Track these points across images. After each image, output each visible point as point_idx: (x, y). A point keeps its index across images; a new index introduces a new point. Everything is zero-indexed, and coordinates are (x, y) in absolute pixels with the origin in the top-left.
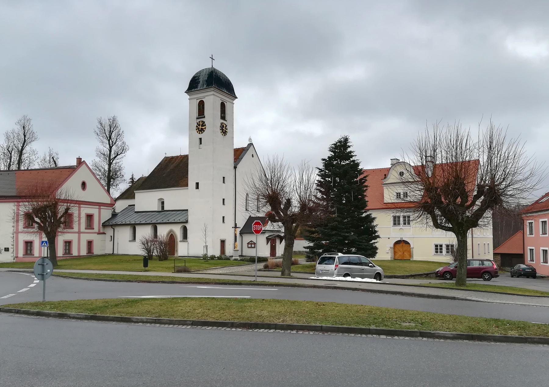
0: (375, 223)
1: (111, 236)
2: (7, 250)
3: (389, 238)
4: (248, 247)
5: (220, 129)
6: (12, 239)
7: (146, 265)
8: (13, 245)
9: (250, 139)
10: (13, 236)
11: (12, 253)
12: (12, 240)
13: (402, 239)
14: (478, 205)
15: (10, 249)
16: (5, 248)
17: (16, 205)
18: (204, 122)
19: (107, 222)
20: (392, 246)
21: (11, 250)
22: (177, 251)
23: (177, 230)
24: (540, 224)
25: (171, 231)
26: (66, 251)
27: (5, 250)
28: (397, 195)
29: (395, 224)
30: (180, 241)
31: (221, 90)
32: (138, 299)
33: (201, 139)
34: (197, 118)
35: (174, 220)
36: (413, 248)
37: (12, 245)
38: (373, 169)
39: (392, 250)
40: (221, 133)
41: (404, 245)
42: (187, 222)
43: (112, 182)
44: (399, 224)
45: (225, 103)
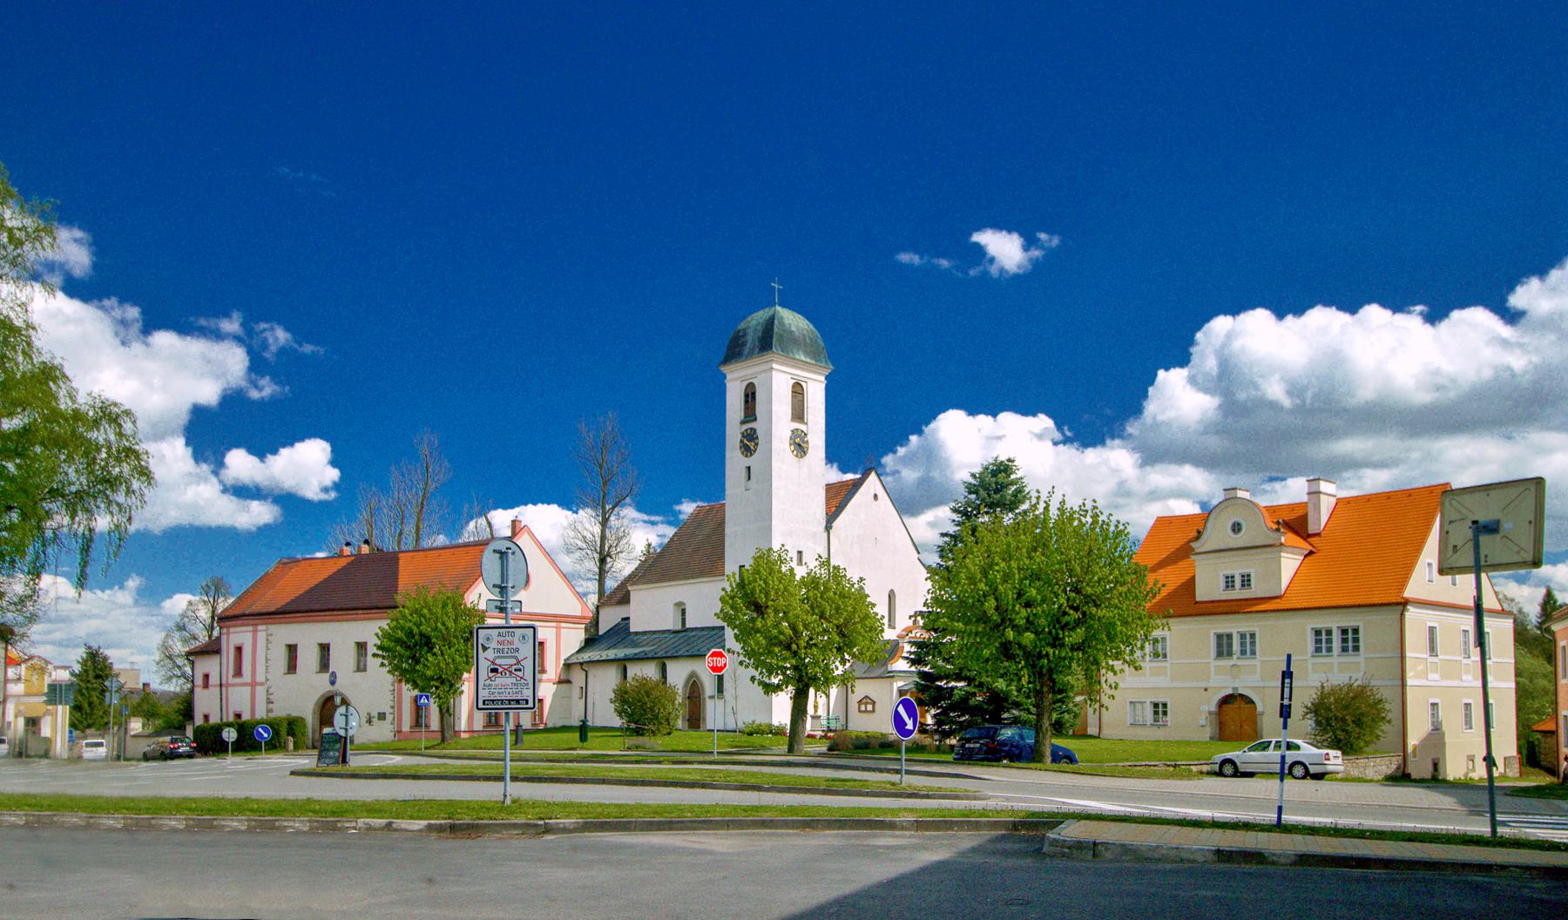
1: (582, 688)
2: (382, 716)
3: (1206, 690)
4: (860, 711)
5: (791, 445)
7: (583, 738)
8: (393, 707)
10: (392, 688)
13: (1235, 692)
16: (379, 713)
18: (755, 430)
19: (573, 658)
20: (1213, 707)
21: (389, 718)
22: (704, 719)
25: (693, 675)
26: (490, 720)
27: (379, 719)
28: (1227, 582)
29: (1220, 654)
30: (712, 697)
31: (792, 356)
34: (743, 423)
35: (698, 650)
36: (1262, 713)
39: (1214, 717)
40: (793, 452)
41: (1243, 705)
43: (609, 565)
44: (1230, 654)
45: (803, 384)
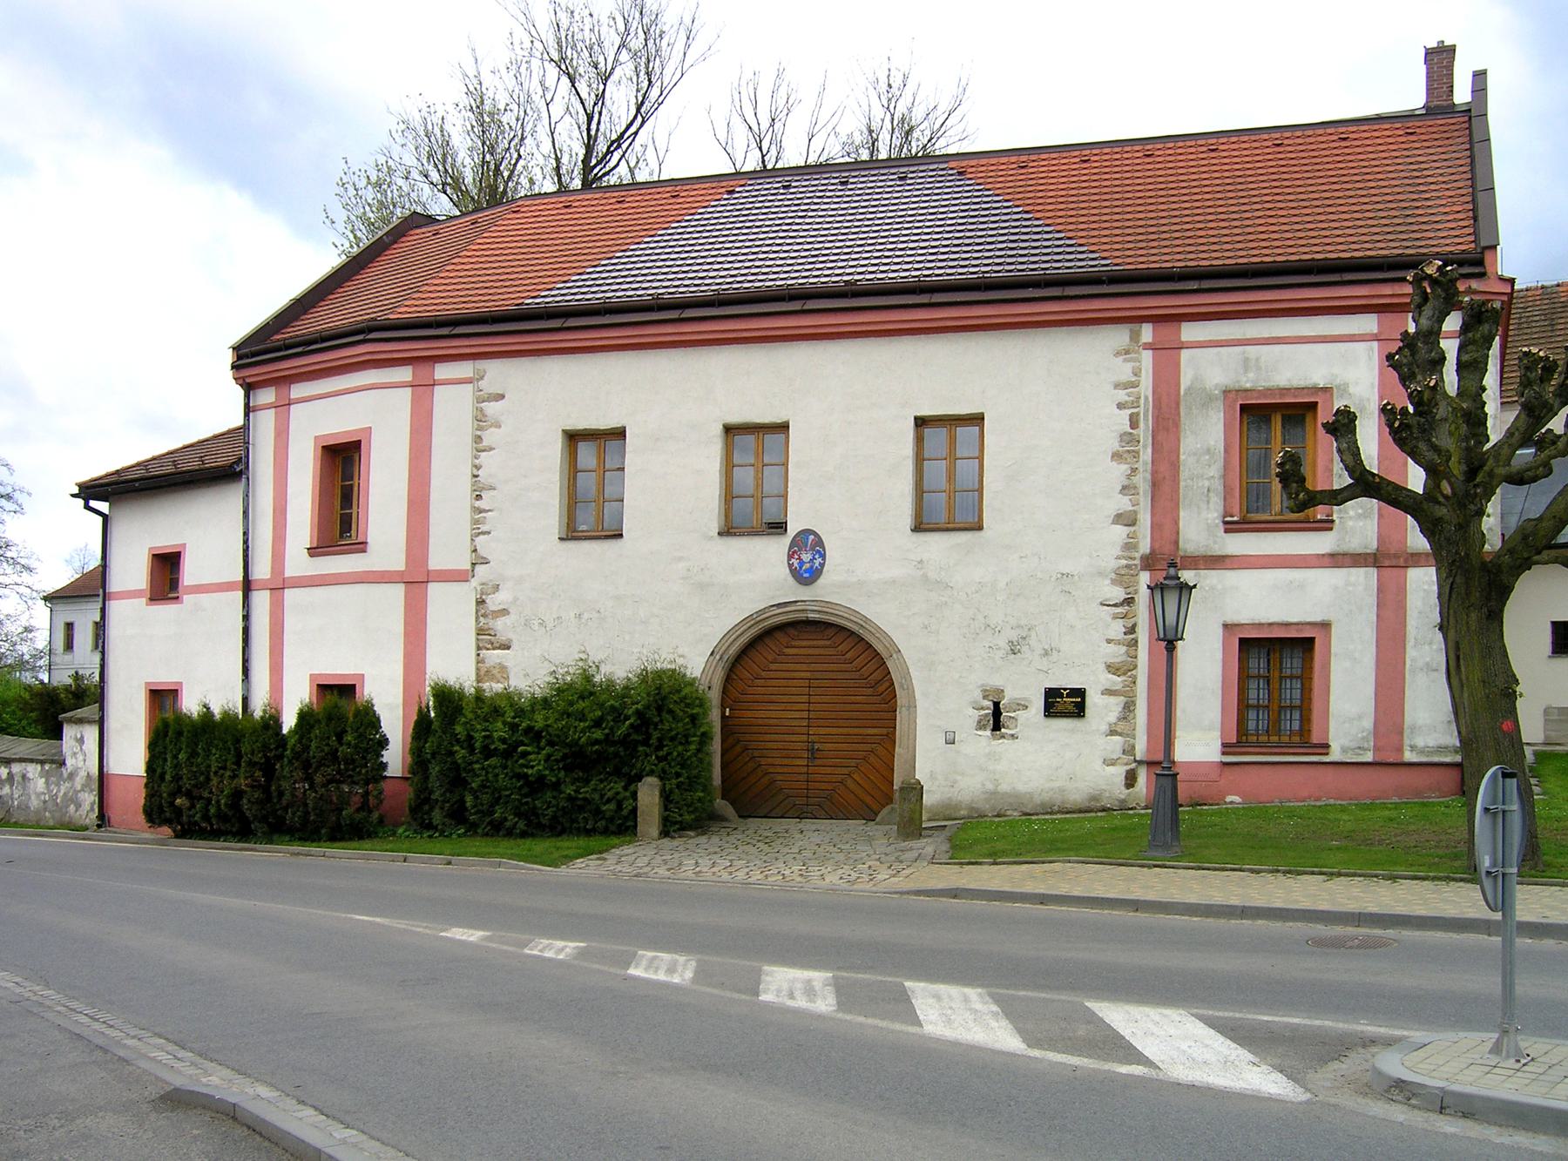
0: (217, 711)
6: (1115, 617)
11: (1112, 733)
12: (1117, 629)
15: (1093, 700)
17: (1147, 347)
21: (1102, 709)
32: (542, 836)
37: (1112, 669)
38: (180, 445)
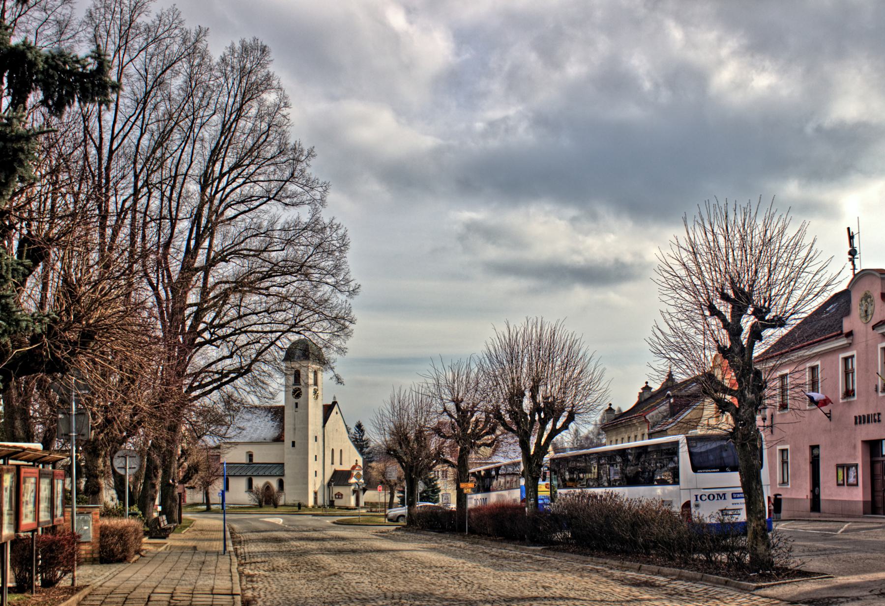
7: (299, 508)
9: (334, 398)
14: (274, 312)
23: (274, 483)
24: (778, 454)
33: (297, 404)
42: (283, 475)
